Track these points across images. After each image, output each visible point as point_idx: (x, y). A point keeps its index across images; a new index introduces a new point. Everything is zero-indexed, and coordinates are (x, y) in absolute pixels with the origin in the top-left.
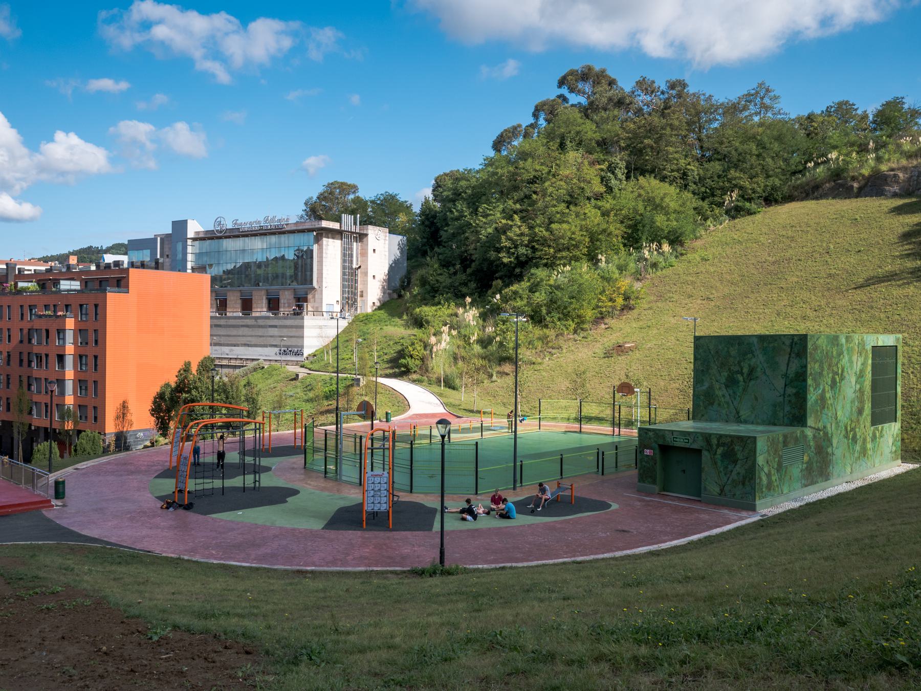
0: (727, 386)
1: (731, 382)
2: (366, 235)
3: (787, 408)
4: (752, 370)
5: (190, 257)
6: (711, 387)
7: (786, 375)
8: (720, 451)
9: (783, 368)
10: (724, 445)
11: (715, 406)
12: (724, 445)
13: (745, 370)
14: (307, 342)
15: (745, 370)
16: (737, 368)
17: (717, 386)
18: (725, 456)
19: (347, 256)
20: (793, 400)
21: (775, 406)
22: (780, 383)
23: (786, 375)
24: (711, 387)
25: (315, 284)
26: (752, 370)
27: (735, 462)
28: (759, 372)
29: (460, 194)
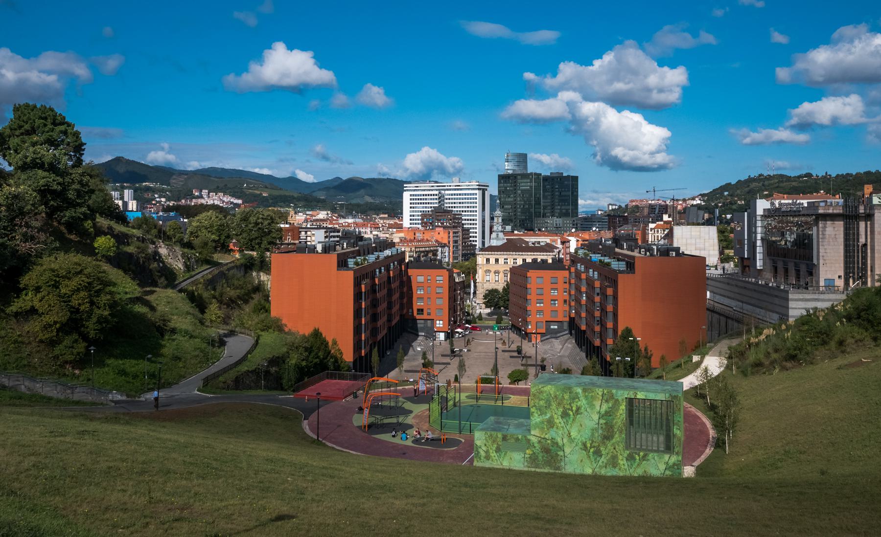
0: (562, 417)
1: (565, 415)
2: (873, 215)
3: (600, 431)
4: (578, 409)
5: (759, 230)
6: (552, 417)
7: (599, 412)
8: (592, 450)
9: (598, 408)
10: (594, 447)
11: (555, 429)
12: (594, 447)
13: (574, 409)
14: (791, 313)
15: (574, 409)
16: (568, 407)
17: (556, 416)
18: (595, 453)
19: (850, 238)
20: (604, 427)
21: (593, 430)
22: (596, 417)
23: (599, 412)
24: (552, 417)
25: (815, 261)
26: (578, 409)
27: (601, 456)
28: (582, 410)
29: (78, 309)
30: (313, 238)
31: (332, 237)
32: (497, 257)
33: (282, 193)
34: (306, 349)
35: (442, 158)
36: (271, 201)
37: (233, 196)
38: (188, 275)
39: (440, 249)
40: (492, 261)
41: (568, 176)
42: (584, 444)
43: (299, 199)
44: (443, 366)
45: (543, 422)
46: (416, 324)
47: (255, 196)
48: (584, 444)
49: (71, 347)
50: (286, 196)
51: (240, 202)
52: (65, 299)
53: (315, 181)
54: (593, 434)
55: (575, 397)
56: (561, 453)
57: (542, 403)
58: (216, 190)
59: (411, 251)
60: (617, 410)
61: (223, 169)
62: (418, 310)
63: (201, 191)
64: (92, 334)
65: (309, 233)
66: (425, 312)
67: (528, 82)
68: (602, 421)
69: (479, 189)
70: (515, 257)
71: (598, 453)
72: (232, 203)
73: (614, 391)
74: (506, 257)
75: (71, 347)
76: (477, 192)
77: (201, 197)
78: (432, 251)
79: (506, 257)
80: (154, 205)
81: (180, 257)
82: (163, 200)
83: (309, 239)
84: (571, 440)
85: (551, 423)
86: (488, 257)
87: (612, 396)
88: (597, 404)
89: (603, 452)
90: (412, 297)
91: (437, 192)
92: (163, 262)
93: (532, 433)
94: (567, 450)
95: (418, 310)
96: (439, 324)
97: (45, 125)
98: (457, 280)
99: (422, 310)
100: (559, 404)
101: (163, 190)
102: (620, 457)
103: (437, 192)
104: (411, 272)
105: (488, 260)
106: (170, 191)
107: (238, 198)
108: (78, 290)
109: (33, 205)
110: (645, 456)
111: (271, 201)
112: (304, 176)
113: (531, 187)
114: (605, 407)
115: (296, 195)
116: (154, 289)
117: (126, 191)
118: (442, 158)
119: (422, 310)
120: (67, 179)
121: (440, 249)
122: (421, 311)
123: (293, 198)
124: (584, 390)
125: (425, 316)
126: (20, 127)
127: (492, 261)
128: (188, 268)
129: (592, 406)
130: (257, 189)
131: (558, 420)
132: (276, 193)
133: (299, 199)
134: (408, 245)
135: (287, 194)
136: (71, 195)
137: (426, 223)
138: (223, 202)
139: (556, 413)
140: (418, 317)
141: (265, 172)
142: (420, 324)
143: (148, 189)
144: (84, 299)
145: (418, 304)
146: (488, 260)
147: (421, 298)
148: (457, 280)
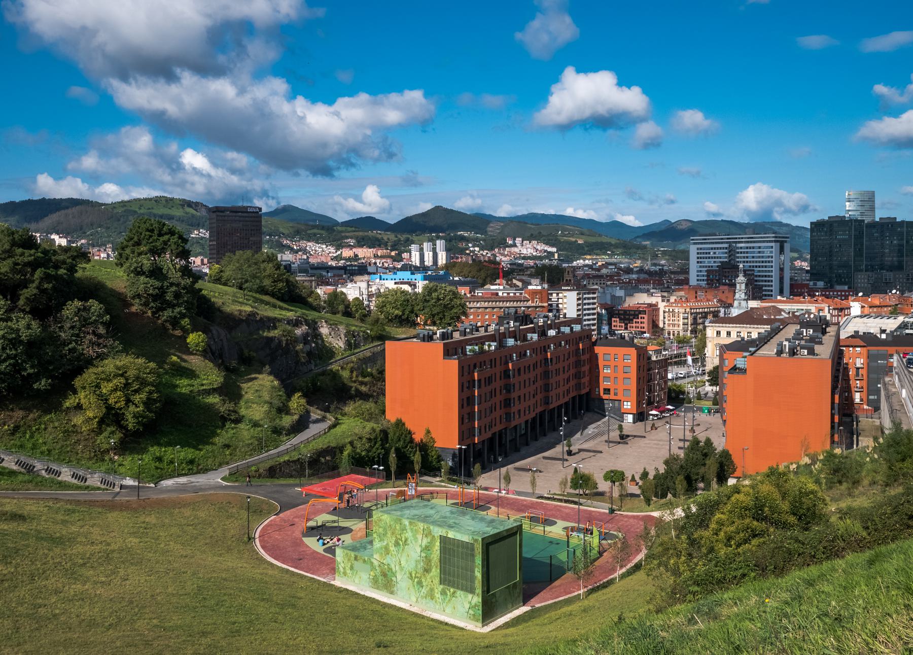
1: (397, 544)
6: (388, 544)
22: (419, 550)
23: (421, 546)
24: (388, 544)
26: (406, 540)
28: (409, 542)
30: (565, 300)
31: (585, 299)
32: (729, 329)
33: (599, 239)
34: (369, 440)
35: (778, 193)
36: (586, 249)
37: (547, 244)
38: (348, 353)
39: (722, 310)
40: (724, 334)
41: (903, 222)
42: (411, 574)
43: (616, 246)
44: (592, 454)
45: (381, 548)
46: (604, 404)
47: (571, 243)
48: (411, 574)
49: (110, 438)
50: (602, 243)
51: (554, 250)
52: (104, 399)
53: (642, 225)
54: (416, 566)
55: (404, 529)
56: (394, 579)
57: (381, 530)
58: (530, 238)
59: (685, 312)
60: (434, 545)
61: (543, 215)
62: (605, 390)
63: (515, 239)
64: (130, 426)
65: (560, 295)
66: (612, 392)
67: (881, 97)
68: (423, 555)
69: (775, 241)
70: (750, 330)
71: (420, 583)
72: (545, 251)
73: (432, 527)
74: (739, 330)
75: (110, 438)
76: (773, 244)
77: (515, 245)
78: (712, 312)
79: (739, 330)
80: (469, 254)
81: (343, 336)
82: (477, 249)
83: (560, 301)
84: (402, 569)
85: (387, 550)
86: (719, 329)
87: (430, 533)
88: (420, 537)
89: (424, 584)
90: (598, 377)
91: (726, 245)
92: (323, 341)
93: (375, 556)
94: (399, 577)
95: (605, 390)
96: (627, 406)
97: (151, 236)
98: (654, 358)
99: (609, 390)
100: (393, 533)
101: (477, 240)
102: (436, 591)
103: (726, 245)
104: (598, 350)
105: (718, 333)
106: (484, 240)
107: (552, 246)
108: (116, 390)
109: (98, 316)
110: (454, 593)
111: (586, 249)
112: (630, 220)
113: (850, 236)
114: (425, 541)
115: (613, 242)
116: (257, 375)
117: (438, 242)
118: (778, 193)
119: (609, 390)
120: (166, 284)
121: (722, 310)
122: (607, 391)
123: (610, 244)
124: (411, 523)
125: (612, 396)
126: (132, 239)
127: (724, 334)
128: (349, 345)
129: (416, 539)
130: (572, 236)
131: (392, 548)
132: (592, 240)
133: (616, 246)
134: (682, 306)
135: (604, 241)
136: (169, 297)
137: (712, 280)
138: (537, 250)
139: (390, 540)
140: (605, 397)
141: (581, 214)
142: (608, 405)
143: (463, 238)
144: (120, 398)
145: (604, 384)
146: (718, 333)
147: (607, 378)
148: (654, 358)
